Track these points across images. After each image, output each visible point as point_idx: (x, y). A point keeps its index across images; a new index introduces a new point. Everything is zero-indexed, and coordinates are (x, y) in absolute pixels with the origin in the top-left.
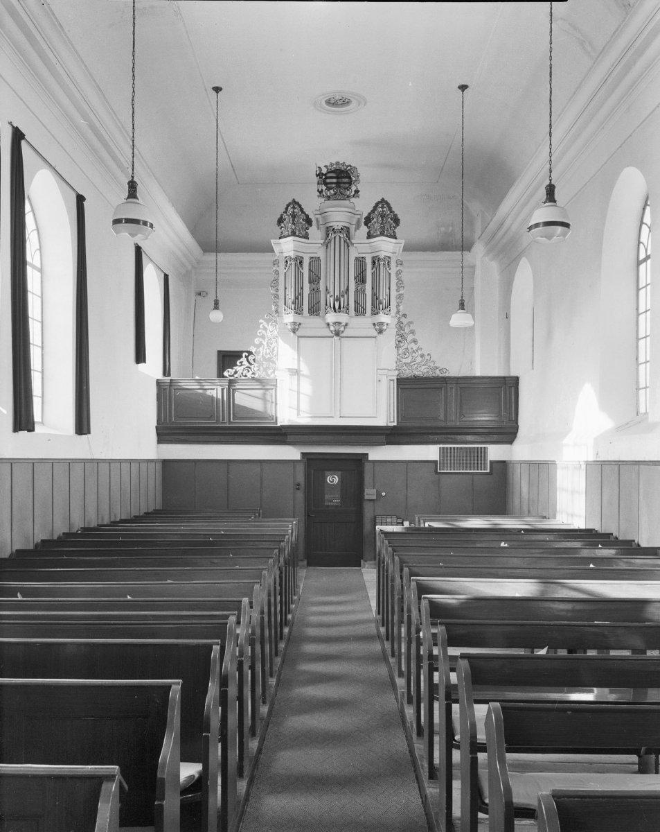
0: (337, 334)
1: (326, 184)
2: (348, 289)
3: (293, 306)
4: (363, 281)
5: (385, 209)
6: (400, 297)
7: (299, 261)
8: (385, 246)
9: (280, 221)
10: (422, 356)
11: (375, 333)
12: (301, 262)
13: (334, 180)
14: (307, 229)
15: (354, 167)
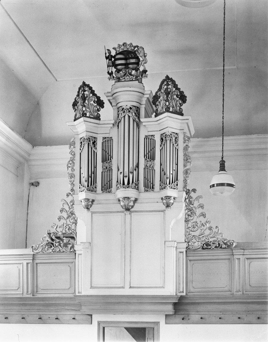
0: (128, 209)
1: (115, 65)
2: (138, 166)
3: (86, 184)
4: (153, 158)
5: (170, 87)
6: (186, 172)
7: (92, 142)
8: (169, 122)
9: (75, 104)
10: (210, 228)
11: (164, 207)
12: (94, 143)
13: (123, 62)
14: (98, 110)
15: (141, 47)
